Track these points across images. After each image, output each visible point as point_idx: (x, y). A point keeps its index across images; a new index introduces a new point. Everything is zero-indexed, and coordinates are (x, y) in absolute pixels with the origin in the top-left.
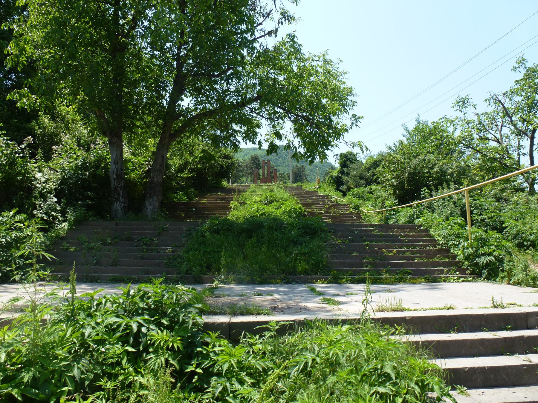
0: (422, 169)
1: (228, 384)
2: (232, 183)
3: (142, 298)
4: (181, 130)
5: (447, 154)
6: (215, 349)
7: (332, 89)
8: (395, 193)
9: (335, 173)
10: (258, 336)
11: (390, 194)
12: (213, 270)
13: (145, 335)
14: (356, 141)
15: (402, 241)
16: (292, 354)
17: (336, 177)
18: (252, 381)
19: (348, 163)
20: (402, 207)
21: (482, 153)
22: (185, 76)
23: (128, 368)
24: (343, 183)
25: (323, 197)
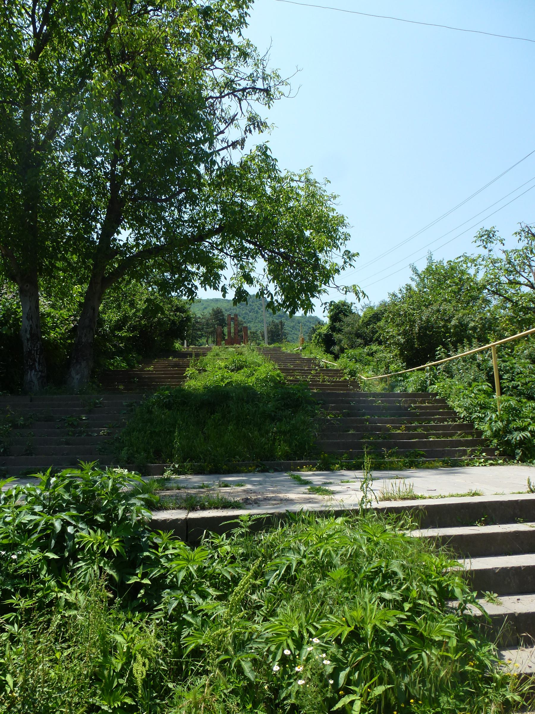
0: (436, 323)
1: (185, 598)
2: (188, 346)
3: (67, 488)
4: (118, 273)
5: (468, 303)
6: (167, 552)
7: (317, 217)
8: (401, 354)
9: (324, 330)
10: (224, 535)
11: (396, 355)
12: (164, 456)
13: (72, 537)
14: (349, 284)
15: (414, 414)
16: (271, 556)
17: (326, 335)
18: (218, 594)
19: (341, 316)
20: (411, 371)
21: (512, 301)
22: (122, 202)
23: (49, 581)
24: (334, 343)
25: (309, 360)
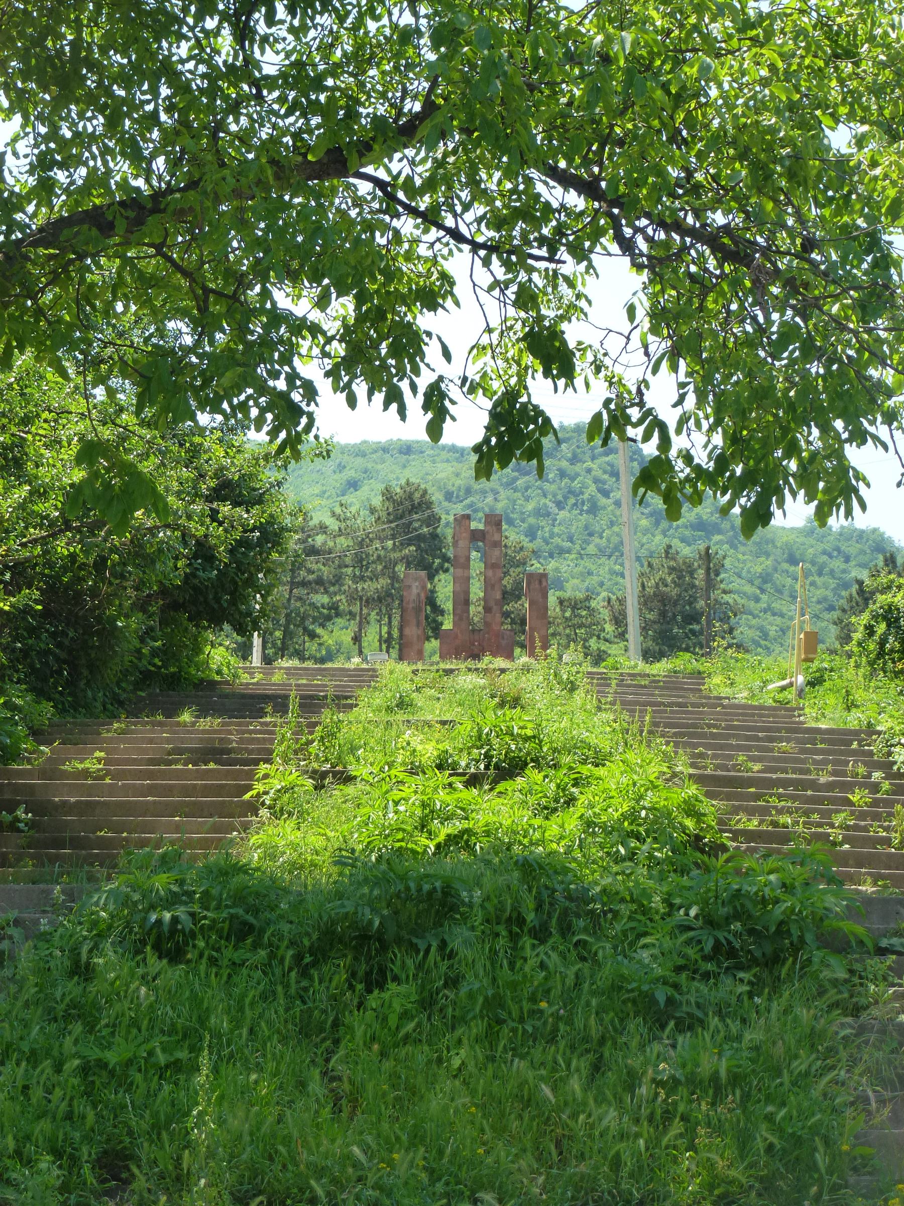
2: (267, 660)
25: (840, 739)
